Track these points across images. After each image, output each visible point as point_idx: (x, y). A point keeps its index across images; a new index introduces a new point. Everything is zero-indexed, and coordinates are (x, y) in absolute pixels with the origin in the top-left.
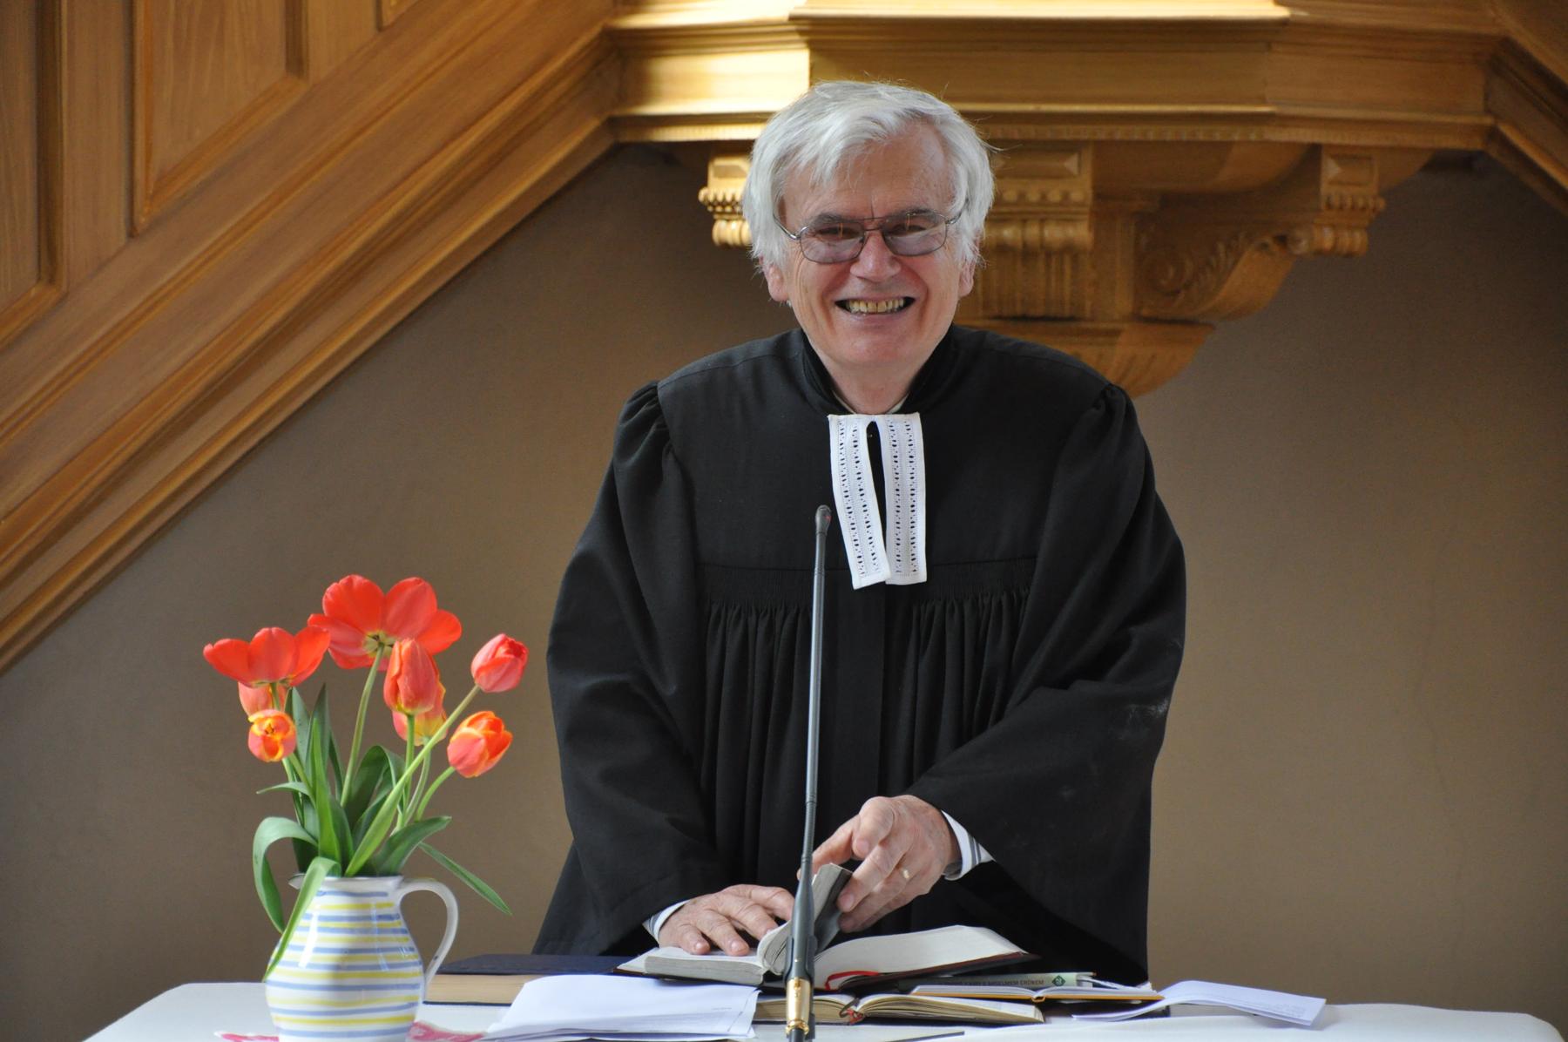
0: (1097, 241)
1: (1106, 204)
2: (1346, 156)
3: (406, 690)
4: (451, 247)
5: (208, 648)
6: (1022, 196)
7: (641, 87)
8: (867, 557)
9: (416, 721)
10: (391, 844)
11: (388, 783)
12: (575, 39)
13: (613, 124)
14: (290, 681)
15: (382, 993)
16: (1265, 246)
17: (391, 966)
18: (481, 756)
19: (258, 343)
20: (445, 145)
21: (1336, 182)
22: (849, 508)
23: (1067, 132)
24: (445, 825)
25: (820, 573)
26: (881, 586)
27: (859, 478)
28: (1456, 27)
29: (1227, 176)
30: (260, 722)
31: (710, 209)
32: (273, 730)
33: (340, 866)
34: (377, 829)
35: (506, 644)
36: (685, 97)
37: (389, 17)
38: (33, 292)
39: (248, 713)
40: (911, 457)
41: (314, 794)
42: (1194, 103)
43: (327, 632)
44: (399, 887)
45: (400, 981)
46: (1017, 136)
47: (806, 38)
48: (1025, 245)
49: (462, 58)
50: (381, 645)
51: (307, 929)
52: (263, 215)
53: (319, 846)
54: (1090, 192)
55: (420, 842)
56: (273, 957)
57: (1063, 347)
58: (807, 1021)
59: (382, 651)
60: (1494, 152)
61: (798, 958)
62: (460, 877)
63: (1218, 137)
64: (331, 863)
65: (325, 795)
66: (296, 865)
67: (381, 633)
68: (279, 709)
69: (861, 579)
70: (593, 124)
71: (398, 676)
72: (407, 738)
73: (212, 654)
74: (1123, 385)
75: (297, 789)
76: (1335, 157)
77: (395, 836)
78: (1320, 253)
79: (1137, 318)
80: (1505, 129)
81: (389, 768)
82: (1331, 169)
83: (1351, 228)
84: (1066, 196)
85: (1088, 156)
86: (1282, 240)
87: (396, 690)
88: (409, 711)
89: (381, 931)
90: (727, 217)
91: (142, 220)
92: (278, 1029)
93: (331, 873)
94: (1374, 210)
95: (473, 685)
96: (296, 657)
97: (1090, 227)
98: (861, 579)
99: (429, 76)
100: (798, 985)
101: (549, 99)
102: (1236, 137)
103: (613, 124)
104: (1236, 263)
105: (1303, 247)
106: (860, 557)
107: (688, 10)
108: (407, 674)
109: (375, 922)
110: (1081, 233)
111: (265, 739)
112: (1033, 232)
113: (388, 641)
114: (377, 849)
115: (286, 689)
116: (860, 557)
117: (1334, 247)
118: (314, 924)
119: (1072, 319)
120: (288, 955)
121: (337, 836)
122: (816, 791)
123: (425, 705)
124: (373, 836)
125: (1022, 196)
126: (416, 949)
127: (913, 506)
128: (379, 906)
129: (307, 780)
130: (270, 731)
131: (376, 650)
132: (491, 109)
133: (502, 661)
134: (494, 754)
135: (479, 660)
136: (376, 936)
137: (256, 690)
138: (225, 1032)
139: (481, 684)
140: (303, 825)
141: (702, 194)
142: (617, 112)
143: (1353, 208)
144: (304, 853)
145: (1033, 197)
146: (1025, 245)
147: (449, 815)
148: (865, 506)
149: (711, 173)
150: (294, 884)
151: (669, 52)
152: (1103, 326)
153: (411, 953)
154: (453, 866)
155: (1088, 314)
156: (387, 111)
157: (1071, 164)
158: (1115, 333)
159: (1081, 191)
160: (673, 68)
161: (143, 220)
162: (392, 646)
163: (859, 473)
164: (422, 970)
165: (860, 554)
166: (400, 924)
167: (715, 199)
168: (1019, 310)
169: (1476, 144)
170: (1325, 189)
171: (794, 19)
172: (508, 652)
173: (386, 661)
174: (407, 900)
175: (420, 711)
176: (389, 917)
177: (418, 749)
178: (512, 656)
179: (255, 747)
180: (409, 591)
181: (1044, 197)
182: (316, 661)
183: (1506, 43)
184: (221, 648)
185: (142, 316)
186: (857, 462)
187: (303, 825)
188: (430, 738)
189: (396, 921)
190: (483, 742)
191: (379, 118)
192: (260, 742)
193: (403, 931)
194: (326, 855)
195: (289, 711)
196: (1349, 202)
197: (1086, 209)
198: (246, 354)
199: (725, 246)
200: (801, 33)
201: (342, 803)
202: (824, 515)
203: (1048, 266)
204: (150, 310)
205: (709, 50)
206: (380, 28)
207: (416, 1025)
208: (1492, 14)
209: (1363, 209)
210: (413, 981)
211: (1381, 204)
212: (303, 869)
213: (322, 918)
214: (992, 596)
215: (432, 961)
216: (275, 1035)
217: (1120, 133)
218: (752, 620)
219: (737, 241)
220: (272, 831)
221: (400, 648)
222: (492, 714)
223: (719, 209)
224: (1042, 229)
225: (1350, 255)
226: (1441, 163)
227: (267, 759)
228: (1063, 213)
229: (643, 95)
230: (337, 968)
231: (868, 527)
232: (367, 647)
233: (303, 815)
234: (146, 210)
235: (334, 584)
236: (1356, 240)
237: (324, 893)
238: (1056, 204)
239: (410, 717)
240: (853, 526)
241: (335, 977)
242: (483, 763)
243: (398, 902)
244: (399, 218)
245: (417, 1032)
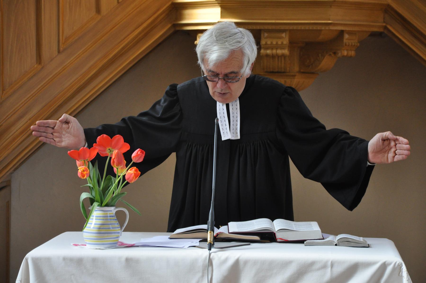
0: (290, 53)
1: (292, 44)
2: (350, 33)
3: (116, 162)
5: (69, 152)
6: (272, 43)
7: (180, 16)
8: (225, 133)
9: (119, 169)
10: (113, 199)
11: (112, 184)
13: (175, 25)
14: (89, 160)
15: (110, 234)
17: (113, 228)
18: (133, 178)
19: (89, 78)
20: (134, 31)
22: (221, 121)
23: (282, 27)
24: (125, 195)
25: (216, 134)
26: (229, 140)
27: (224, 114)
29: (321, 38)
30: (81, 169)
32: (84, 171)
33: (100, 204)
34: (109, 195)
35: (140, 151)
38: (35, 66)
39: (78, 167)
40: (237, 108)
41: (94, 187)
42: (313, 20)
43: (97, 148)
44: (115, 209)
45: (115, 232)
46: (270, 28)
48: (272, 54)
50: (111, 151)
51: (93, 219)
52: (90, 48)
53: (95, 199)
54: (288, 42)
55: (120, 199)
56: (85, 226)
57: (281, 80)
58: (212, 241)
59: (111, 152)
60: (386, 32)
62: (129, 207)
63: (319, 28)
64: (98, 203)
65: (97, 187)
66: (90, 204)
67: (110, 148)
68: (86, 166)
69: (224, 138)
70: (169, 26)
71: (114, 159)
72: (117, 173)
73: (70, 153)
74: (296, 89)
75: (90, 186)
76: (347, 33)
77: (114, 197)
78: (343, 56)
79: (300, 72)
80: (389, 27)
81: (112, 181)
82: (346, 36)
83: (351, 50)
84: (282, 43)
85: (288, 33)
86: (335, 53)
87: (114, 162)
88: (117, 167)
89: (110, 220)
91: (61, 49)
92: (86, 243)
93: (98, 206)
95: (132, 161)
96: (90, 154)
97: (288, 50)
98: (224, 138)
100: (210, 232)
101: (159, 20)
102: (323, 28)
103: (175, 25)
104: (324, 58)
106: (224, 133)
108: (116, 158)
109: (109, 218)
110: (286, 52)
111: (82, 173)
112: (274, 51)
113: (112, 150)
114: (109, 200)
115: (88, 162)
116: (224, 133)
118: (94, 218)
119: (284, 72)
120: (88, 225)
121: (100, 197)
122: (215, 186)
123: (121, 166)
124: (108, 197)
125: (272, 43)
126: (119, 224)
127: (237, 120)
128: (110, 214)
129: (92, 184)
130: (83, 171)
131: (109, 152)
132: (145, 22)
133: (139, 154)
134: (136, 177)
135: (134, 155)
136: (109, 221)
137: (80, 162)
138: (73, 244)
139: (134, 160)
140: (92, 194)
143: (352, 45)
144: (92, 201)
145: (274, 43)
146: (272, 54)
147: (126, 192)
148: (225, 120)
149: (198, 37)
150: (89, 208)
151: (188, 8)
152: (291, 74)
153: (118, 225)
154: (128, 204)
155: (288, 71)
157: (284, 35)
158: (294, 76)
159: (286, 41)
161: (61, 49)
162: (113, 151)
163: (224, 112)
164: (120, 229)
165: (224, 132)
166: (115, 218)
168: (271, 70)
169: (382, 30)
170: (345, 41)
172: (140, 153)
173: (112, 155)
174: (117, 212)
175: (120, 167)
176: (112, 216)
177: (119, 176)
178: (141, 154)
179: (79, 175)
180: (117, 138)
181: (277, 43)
182: (95, 155)
183: (389, 6)
184: (72, 152)
185: (61, 72)
186: (223, 110)
187: (92, 194)
188: (122, 173)
189: (114, 217)
190: (133, 174)
191: (118, 24)
192: (80, 174)
193: (116, 220)
194: (97, 202)
195: (89, 167)
196: (350, 44)
197: (287, 46)
200: (219, 3)
201: (101, 189)
203: (278, 60)
204: (63, 70)
205: (197, 8)
207: (119, 242)
209: (354, 46)
210: (118, 231)
211: (359, 44)
212: (92, 205)
213: (96, 217)
214: (257, 141)
215: (123, 227)
216: (85, 244)
217: (295, 27)
218: (198, 147)
220: (84, 196)
221: (115, 152)
222: (135, 168)
224: (276, 51)
226: (373, 34)
227: (83, 178)
228: (282, 47)
230: (99, 228)
231: (226, 125)
232: (107, 151)
233: (92, 191)
234: (62, 46)
235: (99, 137)
236: (353, 53)
237: (97, 211)
238: (280, 45)
239: (117, 169)
240: (222, 125)
241: (99, 230)
242: (134, 179)
243: (114, 213)
244: (123, 48)
245: (119, 244)
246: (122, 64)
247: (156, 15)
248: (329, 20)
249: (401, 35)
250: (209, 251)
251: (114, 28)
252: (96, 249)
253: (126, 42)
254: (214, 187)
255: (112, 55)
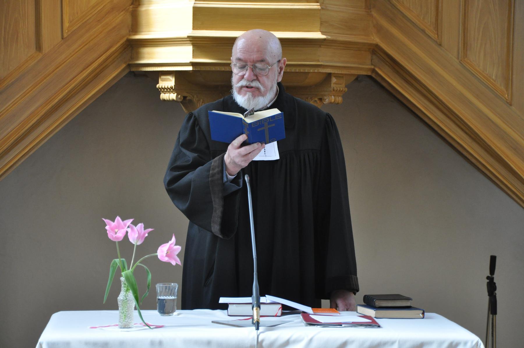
2: (337, 76)
4: (85, 99)
7: (138, 56)
12: (118, 42)
16: (316, 101)
21: (335, 83)
25: (250, 194)
28: (366, 41)
31: (160, 90)
36: (152, 58)
37: (65, 35)
47: (191, 42)
49: (86, 47)
52: (29, 92)
61: (256, 301)
70: (124, 66)
76: (334, 76)
78: (331, 103)
80: (377, 69)
82: (334, 80)
83: (338, 96)
86: (321, 99)
90: (165, 92)
94: (344, 91)
99: (76, 52)
101: (110, 59)
103: (129, 66)
105: (327, 101)
107: (148, 34)
117: (334, 101)
138: (90, 327)
141: (157, 86)
142: (130, 63)
149: (160, 80)
156: (65, 62)
160: (146, 50)
167: (162, 87)
169: (369, 73)
171: (188, 37)
183: (377, 46)
196: (344, 90)
198: (26, 131)
199: (164, 100)
200: (190, 41)
202: (247, 177)
206: (63, 38)
208: (373, 38)
211: (346, 89)
219: (168, 99)
223: (162, 90)
225: (338, 103)
226: (358, 79)
229: (138, 58)
236: (340, 99)
244: (70, 92)
246: (68, 110)
247: (108, 53)
248: (318, 61)
249: (391, 79)
250: (257, 330)
251: (57, 68)
252: (121, 331)
253: (73, 85)
254: (255, 256)
255: (57, 100)
